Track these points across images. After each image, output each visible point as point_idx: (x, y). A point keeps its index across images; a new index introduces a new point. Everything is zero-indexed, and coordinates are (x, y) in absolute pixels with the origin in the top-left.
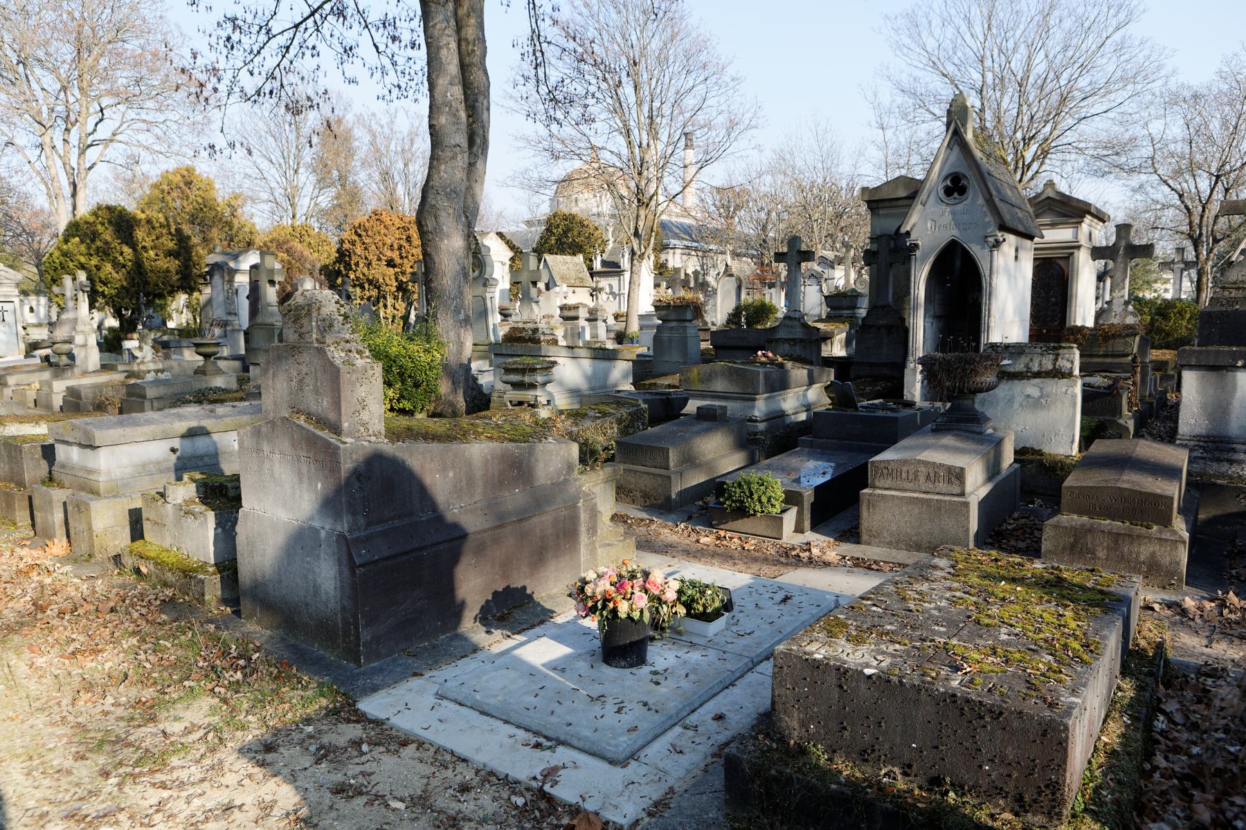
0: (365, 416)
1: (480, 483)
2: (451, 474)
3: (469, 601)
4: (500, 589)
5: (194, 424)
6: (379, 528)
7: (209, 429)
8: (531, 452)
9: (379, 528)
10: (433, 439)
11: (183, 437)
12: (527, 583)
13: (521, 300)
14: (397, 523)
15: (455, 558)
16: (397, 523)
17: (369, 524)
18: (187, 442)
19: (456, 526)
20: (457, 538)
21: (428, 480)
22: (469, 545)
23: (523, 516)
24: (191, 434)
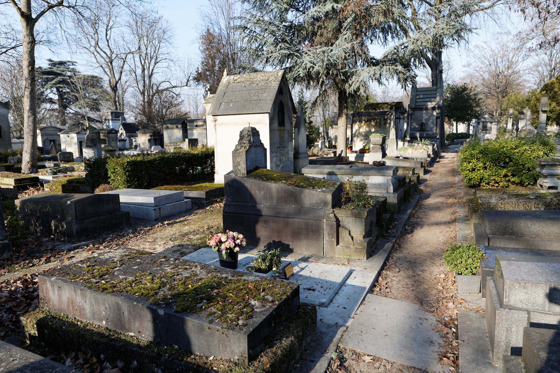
0: (239, 167)
1: (35, 176)
2: (262, 192)
3: (262, 239)
4: (277, 241)
5: (331, 170)
6: (234, 203)
7: (336, 173)
8: (301, 192)
9: (234, 203)
10: (272, 180)
11: (327, 174)
12: (290, 243)
13: (409, 142)
14: (241, 203)
15: (256, 222)
16: (241, 203)
17: (232, 201)
18: (329, 176)
19: (259, 211)
20: (258, 215)
21: (253, 192)
22: (261, 219)
23: (288, 216)
24: (330, 174)
